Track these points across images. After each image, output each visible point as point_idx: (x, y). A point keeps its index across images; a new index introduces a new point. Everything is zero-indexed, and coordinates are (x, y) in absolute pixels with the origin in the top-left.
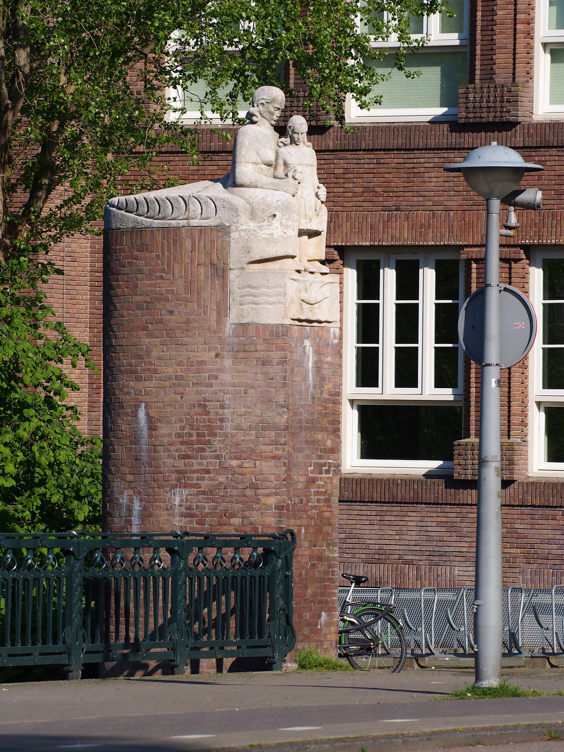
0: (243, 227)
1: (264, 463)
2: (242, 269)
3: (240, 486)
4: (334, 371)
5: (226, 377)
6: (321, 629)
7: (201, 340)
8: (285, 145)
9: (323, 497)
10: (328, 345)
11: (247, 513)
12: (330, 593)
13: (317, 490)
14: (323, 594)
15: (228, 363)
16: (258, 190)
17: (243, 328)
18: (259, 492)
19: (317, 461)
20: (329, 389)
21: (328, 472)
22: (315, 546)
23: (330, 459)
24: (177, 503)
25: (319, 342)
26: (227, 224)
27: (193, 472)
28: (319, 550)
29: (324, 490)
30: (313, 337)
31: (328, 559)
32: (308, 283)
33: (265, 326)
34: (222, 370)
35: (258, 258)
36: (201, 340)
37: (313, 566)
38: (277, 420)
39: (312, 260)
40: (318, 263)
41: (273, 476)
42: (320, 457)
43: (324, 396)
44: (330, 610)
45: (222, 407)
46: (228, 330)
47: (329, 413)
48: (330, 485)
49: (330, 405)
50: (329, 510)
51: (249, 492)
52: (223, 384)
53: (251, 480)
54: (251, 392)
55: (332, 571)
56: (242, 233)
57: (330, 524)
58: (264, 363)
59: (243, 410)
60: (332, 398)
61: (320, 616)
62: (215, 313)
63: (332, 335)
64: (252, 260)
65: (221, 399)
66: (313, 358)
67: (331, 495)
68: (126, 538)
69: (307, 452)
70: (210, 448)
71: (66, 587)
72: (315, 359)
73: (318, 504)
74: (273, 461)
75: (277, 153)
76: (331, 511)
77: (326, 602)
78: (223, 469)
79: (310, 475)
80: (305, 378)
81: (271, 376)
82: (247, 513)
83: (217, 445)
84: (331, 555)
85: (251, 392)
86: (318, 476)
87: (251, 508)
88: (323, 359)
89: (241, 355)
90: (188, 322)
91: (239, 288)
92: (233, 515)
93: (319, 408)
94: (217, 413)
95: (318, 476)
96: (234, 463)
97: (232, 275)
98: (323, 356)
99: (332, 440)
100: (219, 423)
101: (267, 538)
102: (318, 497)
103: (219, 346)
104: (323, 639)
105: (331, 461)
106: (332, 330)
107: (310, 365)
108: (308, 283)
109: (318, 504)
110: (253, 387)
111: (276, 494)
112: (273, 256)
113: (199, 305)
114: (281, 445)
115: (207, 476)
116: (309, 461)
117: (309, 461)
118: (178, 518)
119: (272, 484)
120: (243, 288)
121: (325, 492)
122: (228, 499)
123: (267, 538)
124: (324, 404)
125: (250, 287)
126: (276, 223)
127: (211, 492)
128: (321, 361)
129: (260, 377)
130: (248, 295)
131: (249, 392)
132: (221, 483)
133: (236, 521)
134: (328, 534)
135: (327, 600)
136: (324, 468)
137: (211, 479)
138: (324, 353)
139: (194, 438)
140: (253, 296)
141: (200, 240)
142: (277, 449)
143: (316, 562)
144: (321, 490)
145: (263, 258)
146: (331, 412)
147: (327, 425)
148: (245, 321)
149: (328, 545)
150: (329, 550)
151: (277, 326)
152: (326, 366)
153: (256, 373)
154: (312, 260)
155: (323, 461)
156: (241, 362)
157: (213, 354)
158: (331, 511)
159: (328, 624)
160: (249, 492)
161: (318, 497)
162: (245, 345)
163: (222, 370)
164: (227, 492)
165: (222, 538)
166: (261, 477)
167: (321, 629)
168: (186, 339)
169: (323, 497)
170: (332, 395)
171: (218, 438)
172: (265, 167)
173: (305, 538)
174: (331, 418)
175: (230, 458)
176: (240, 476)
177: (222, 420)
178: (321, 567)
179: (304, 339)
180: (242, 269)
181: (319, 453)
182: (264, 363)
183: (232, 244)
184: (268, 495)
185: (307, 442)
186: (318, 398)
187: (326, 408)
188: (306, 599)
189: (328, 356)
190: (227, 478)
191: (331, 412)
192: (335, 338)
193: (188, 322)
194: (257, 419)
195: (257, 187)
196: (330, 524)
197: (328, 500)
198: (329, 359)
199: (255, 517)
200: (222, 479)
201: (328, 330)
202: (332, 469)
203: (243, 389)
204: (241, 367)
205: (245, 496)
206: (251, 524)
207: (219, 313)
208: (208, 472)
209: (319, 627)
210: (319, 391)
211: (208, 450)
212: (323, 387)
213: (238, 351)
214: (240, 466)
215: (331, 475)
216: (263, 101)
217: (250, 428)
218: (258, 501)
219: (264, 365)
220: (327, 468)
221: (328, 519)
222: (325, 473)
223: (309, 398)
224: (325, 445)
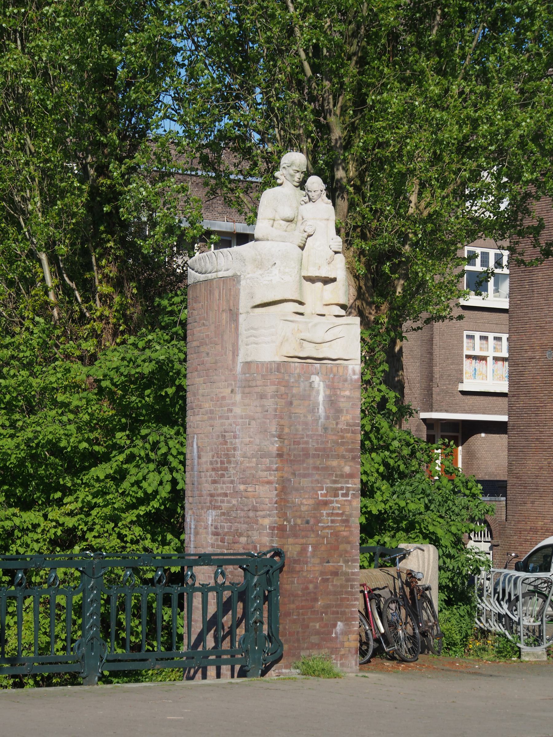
0: (249, 276)
1: (261, 488)
2: (248, 312)
3: (246, 509)
4: (353, 404)
5: (238, 410)
6: (337, 637)
7: (223, 377)
8: (306, 203)
10: (345, 380)
11: (250, 533)
12: (348, 605)
14: (339, 606)
15: (238, 397)
16: (269, 242)
17: (248, 364)
18: (260, 513)
22: (328, 562)
24: (210, 523)
25: (333, 378)
26: (239, 274)
27: (219, 495)
28: (333, 566)
29: (341, 512)
30: (325, 373)
31: (346, 574)
32: (310, 325)
33: (263, 363)
34: (234, 404)
35: (259, 302)
36: (223, 377)
37: (325, 581)
38: (270, 448)
39: (329, 305)
40: (339, 308)
41: (267, 500)
42: (335, 482)
43: (340, 426)
44: (348, 621)
45: (235, 437)
46: (239, 368)
47: (347, 442)
48: (348, 507)
49: (349, 435)
51: (251, 514)
52: (235, 417)
53: (253, 503)
54: (253, 423)
56: (248, 281)
57: (348, 542)
58: (262, 396)
59: (248, 439)
60: (351, 428)
61: (335, 626)
62: (231, 353)
63: (350, 371)
64: (255, 304)
65: (234, 430)
66: (324, 392)
69: (317, 477)
70: (227, 474)
72: (328, 392)
74: (268, 486)
76: (350, 531)
77: (344, 613)
78: (236, 493)
79: (320, 498)
80: (313, 409)
81: (266, 408)
82: (250, 533)
83: (232, 471)
84: (350, 571)
85: (253, 423)
86: (332, 499)
87: (252, 529)
88: (338, 393)
89: (247, 390)
90: (216, 363)
91: (246, 330)
92: (241, 535)
93: (334, 438)
94: (231, 443)
95: (332, 499)
96: (242, 487)
97: (241, 318)
99: (350, 466)
100: (233, 452)
101: (245, 557)
102: (333, 518)
103: (233, 383)
104: (339, 646)
105: (350, 485)
106: (350, 367)
107: (321, 398)
108: (310, 325)
110: (254, 419)
111: (269, 515)
112: (271, 300)
113: (222, 347)
114: (274, 471)
115: (225, 499)
116: (319, 485)
117: (319, 485)
118: (210, 536)
119: (267, 507)
120: (249, 330)
121: (342, 514)
122: (238, 520)
123: (245, 557)
124: (340, 434)
125: (253, 328)
126: (275, 270)
127: (228, 513)
128: (336, 395)
129: (259, 409)
130: (251, 336)
131: (252, 423)
132: (234, 505)
133: (243, 540)
134: (346, 552)
135: (345, 611)
136: (340, 492)
137: (229, 502)
138: (340, 387)
139: (219, 465)
140: (254, 336)
141: (223, 289)
142: (270, 475)
144: (335, 512)
145: (263, 302)
146: (350, 441)
147: (344, 453)
148: (249, 359)
149: (346, 562)
150: (347, 566)
151: (271, 363)
152: (342, 400)
153: (256, 406)
154: (329, 305)
155: (339, 485)
156: (247, 397)
157: (230, 390)
158: (350, 531)
159: (345, 633)
160: (251, 514)
161: (333, 518)
162: (249, 381)
163: (234, 404)
164: (237, 514)
165: (217, 557)
166: (259, 500)
167: (337, 637)
168: (215, 377)
170: (351, 426)
171: (233, 465)
172: (284, 222)
173: (314, 555)
174: (350, 447)
175: (240, 483)
176: (245, 499)
177: (235, 449)
178: (337, 582)
179: (313, 374)
180: (248, 312)
182: (262, 396)
183: (241, 291)
184: (264, 517)
185: (316, 468)
186: (333, 429)
187: (343, 437)
188: (315, 611)
189: (345, 391)
190: (238, 501)
192: (354, 373)
193: (216, 363)
194: (256, 448)
195: (268, 240)
196: (348, 542)
197: (347, 521)
198: (347, 393)
199: (255, 537)
200: (234, 502)
201: (346, 367)
202: (351, 492)
203: (247, 420)
204: (247, 401)
205: (248, 517)
206: (253, 542)
207: (233, 353)
208: (226, 495)
209: (334, 635)
210: (334, 422)
211: (226, 476)
213: (245, 387)
214: (246, 491)
215: (349, 498)
216: (285, 165)
217: (253, 456)
218: (256, 522)
219: (261, 398)
220: (344, 492)
221: (347, 537)
223: (320, 428)
224: (342, 471)
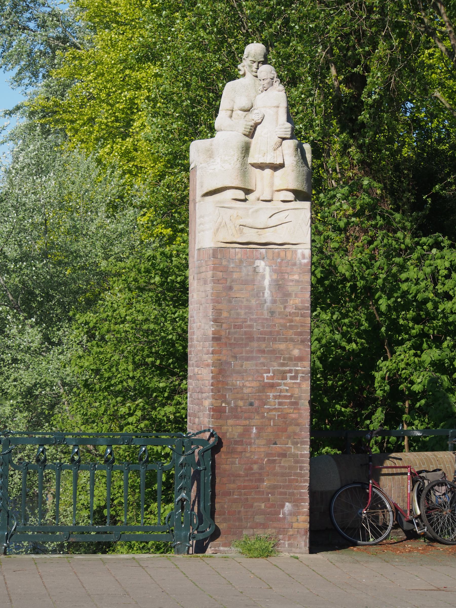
4: (302, 288)
6: (284, 518)
9: (288, 401)
10: (294, 264)
12: (297, 486)
13: (278, 394)
19: (279, 368)
20: (296, 304)
21: (295, 378)
23: (298, 367)
25: (280, 263)
29: (289, 394)
31: (295, 456)
42: (283, 365)
43: (288, 310)
50: (295, 412)
55: (300, 466)
60: (300, 312)
61: (283, 506)
66: (271, 276)
67: (300, 398)
68: (84, 437)
71: (86, 439)
73: (280, 407)
75: (245, 181)
88: (286, 277)
98: (286, 274)
105: (299, 368)
106: (299, 251)
109: (280, 407)
121: (291, 397)
128: (284, 279)
143: (276, 458)
146: (299, 324)
152: (291, 284)
155: (288, 368)
167: (284, 518)
169: (288, 401)
181: (282, 361)
186: (280, 313)
191: (299, 324)
196: (298, 425)
198: (296, 277)
201: (295, 252)
202: (300, 375)
210: (282, 306)
212: (286, 301)
215: (298, 381)
220: (293, 374)
222: (292, 370)
